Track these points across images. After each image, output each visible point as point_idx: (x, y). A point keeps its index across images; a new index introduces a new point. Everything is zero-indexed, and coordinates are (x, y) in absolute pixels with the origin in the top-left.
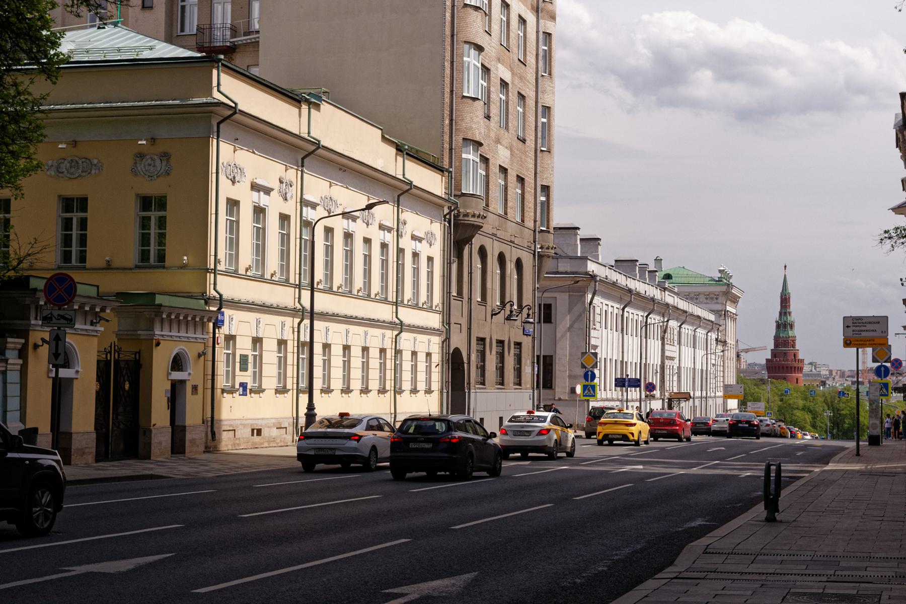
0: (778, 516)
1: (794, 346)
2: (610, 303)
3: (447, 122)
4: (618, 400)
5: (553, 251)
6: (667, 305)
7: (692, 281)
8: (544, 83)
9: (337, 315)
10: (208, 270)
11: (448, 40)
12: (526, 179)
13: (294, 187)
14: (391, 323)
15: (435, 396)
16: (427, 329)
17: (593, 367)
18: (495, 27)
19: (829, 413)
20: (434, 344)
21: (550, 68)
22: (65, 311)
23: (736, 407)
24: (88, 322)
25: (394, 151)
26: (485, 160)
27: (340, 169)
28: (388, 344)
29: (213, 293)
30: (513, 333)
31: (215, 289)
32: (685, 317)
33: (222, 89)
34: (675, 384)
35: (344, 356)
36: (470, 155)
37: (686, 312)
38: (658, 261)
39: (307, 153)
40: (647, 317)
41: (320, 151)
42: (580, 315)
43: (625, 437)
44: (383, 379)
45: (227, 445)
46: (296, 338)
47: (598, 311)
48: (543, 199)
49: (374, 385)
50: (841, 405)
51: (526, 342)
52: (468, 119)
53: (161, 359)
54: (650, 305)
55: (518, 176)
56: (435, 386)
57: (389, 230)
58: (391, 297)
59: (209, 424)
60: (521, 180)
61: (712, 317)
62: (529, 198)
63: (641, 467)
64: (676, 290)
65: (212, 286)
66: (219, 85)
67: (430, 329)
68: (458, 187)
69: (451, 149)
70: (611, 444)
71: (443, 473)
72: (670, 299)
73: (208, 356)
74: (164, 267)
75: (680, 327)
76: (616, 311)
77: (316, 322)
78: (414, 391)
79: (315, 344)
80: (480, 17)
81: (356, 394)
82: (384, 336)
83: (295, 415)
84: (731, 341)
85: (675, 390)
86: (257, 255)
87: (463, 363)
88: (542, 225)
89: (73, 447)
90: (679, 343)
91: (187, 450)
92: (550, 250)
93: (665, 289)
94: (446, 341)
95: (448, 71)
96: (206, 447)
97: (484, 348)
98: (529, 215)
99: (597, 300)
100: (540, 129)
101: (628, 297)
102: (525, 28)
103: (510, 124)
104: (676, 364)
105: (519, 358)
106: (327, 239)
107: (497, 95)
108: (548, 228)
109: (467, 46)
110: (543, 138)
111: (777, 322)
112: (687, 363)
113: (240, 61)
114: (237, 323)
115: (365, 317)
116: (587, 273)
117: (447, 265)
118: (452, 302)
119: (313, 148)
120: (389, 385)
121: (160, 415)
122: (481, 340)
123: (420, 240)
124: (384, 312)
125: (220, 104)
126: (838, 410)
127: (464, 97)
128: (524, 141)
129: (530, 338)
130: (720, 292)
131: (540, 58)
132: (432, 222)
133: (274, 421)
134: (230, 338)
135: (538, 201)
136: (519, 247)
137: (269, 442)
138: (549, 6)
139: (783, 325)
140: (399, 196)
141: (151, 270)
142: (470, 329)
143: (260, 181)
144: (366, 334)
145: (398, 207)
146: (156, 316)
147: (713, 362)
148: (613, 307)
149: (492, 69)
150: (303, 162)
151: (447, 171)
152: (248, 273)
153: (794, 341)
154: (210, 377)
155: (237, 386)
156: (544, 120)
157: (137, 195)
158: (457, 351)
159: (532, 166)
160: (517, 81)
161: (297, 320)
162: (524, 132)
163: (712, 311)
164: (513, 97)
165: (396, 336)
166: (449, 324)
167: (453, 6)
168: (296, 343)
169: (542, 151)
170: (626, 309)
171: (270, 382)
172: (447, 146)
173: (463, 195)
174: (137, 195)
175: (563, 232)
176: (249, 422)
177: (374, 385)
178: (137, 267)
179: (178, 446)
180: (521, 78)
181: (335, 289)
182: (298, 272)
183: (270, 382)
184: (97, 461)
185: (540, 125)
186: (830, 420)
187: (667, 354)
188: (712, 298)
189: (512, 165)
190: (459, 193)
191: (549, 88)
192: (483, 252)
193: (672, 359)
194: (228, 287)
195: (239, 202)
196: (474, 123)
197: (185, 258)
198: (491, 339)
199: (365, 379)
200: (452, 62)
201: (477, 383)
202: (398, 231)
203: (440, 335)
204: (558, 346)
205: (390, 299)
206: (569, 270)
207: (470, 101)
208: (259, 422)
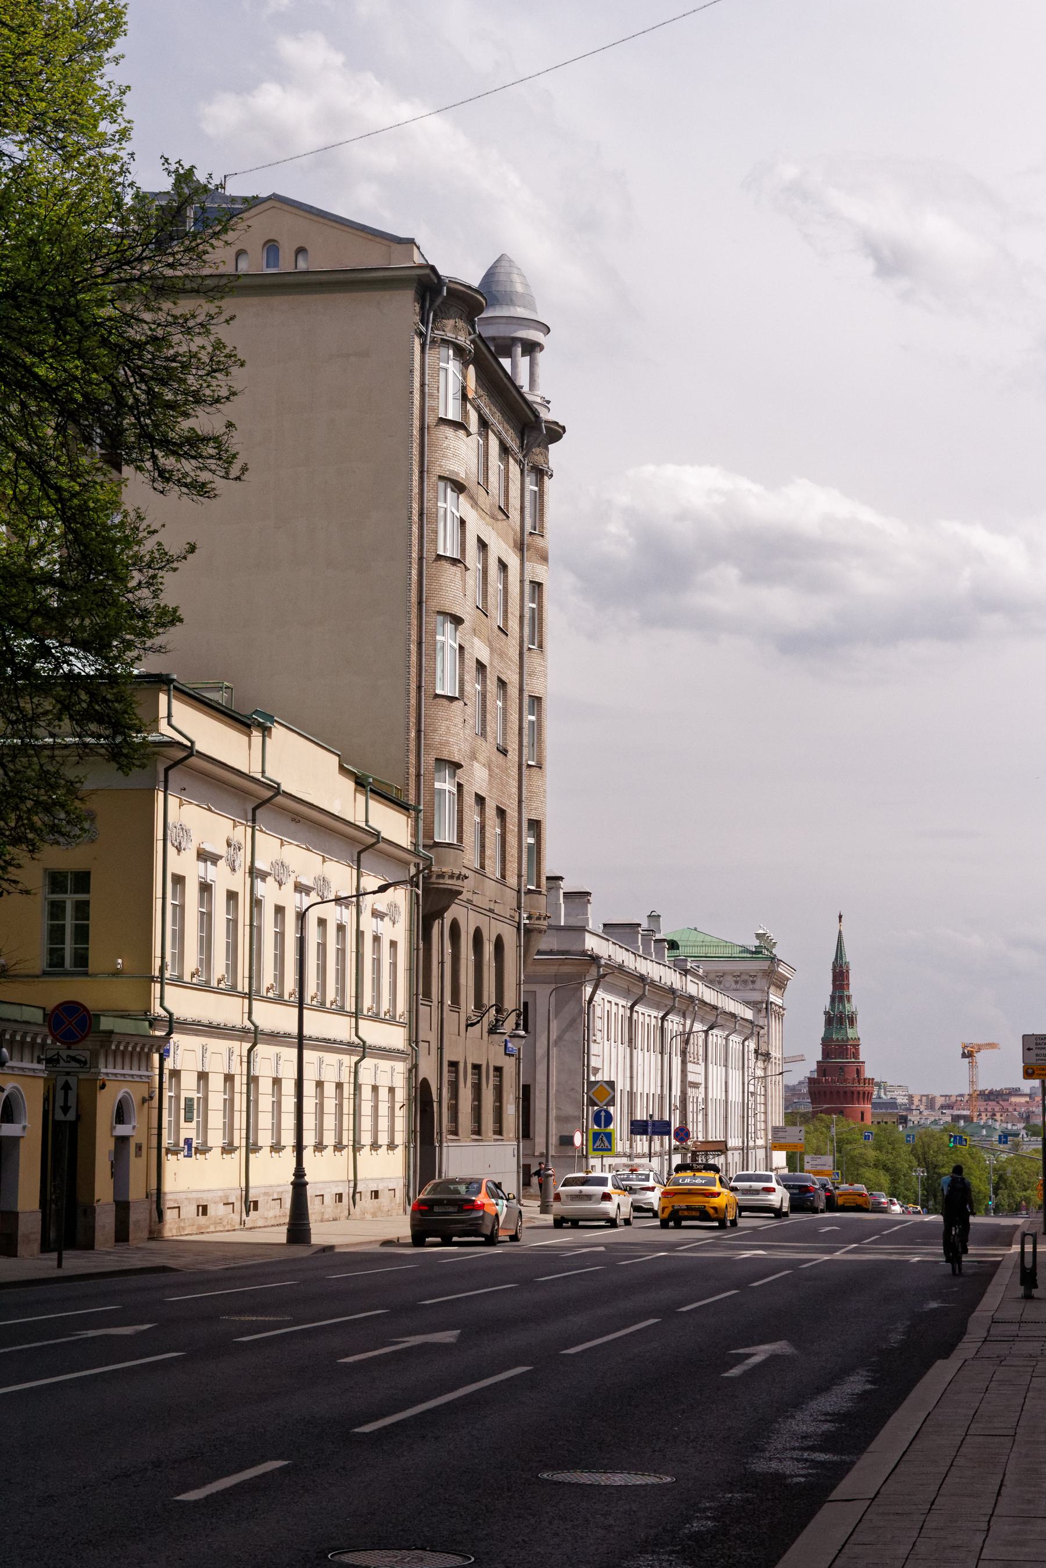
0: (1035, 1292)
1: (856, 1055)
2: (614, 999)
3: (413, 734)
4: (625, 1155)
5: (545, 923)
6: (691, 998)
7: (711, 952)
8: (532, 660)
10: (152, 979)
11: (414, 610)
12: (508, 811)
14: (349, 1044)
15: (400, 1152)
17: (608, 1105)
19: (921, 1173)
22: (81, 1051)
23: (784, 1164)
24: (35, 1061)
25: (351, 785)
27: (293, 820)
31: (162, 1005)
32: (716, 1018)
33: (174, 722)
36: (445, 785)
37: (715, 1008)
38: (654, 918)
39: (259, 801)
40: (663, 1019)
41: (193, 760)
42: (573, 1021)
43: (703, 1215)
44: (229, 1128)
45: (171, 1230)
46: (245, 1072)
47: (598, 1012)
48: (531, 840)
50: (940, 1157)
53: (105, 1105)
54: (672, 1001)
56: (400, 1138)
59: (154, 1198)
61: (749, 1014)
62: (512, 840)
65: (158, 1001)
66: (169, 716)
68: (429, 833)
69: (418, 775)
70: (678, 1226)
73: (153, 1099)
74: (86, 974)
77: (306, 1052)
78: (375, 1146)
79: (305, 1082)
80: (459, 574)
83: (243, 1185)
84: (775, 1053)
87: (432, 1101)
88: (529, 882)
89: (20, 1233)
91: (131, 1238)
92: (542, 922)
94: (414, 1069)
95: (414, 658)
96: (151, 1232)
98: (512, 866)
100: (526, 731)
101: (639, 989)
103: (488, 729)
108: (538, 886)
109: (440, 618)
111: (826, 1013)
112: (716, 1092)
114: (186, 1053)
116: (584, 953)
117: (413, 950)
119: (270, 794)
120: (239, 1139)
121: (103, 1190)
122: (454, 1065)
125: (173, 744)
126: (936, 1166)
127: (437, 696)
128: (504, 752)
129: (513, 1059)
130: (759, 970)
131: (526, 621)
132: (324, 861)
133: (220, 1193)
134: (175, 1074)
135: (524, 845)
136: (499, 918)
137: (215, 1224)
139: (838, 1018)
140: (359, 853)
141: (68, 979)
142: (441, 1048)
145: (358, 869)
146: (101, 1046)
147: (751, 1089)
152: (221, 986)
153: (856, 1047)
154: (155, 1131)
155: (182, 1144)
157: (45, 870)
159: (515, 790)
161: (247, 1046)
163: (747, 1003)
164: (492, 686)
165: (356, 1064)
167: (421, 559)
169: (529, 766)
171: (216, 1139)
172: (412, 771)
173: (437, 845)
174: (45, 870)
176: (194, 1195)
178: (45, 973)
179: (122, 1234)
180: (502, 655)
181: (214, 983)
183: (216, 1139)
184: (42, 1252)
185: (525, 725)
186: (923, 1185)
187: (691, 1078)
188: (745, 982)
189: (490, 791)
190: (431, 842)
191: (539, 668)
193: (696, 1085)
194: (181, 1002)
197: (120, 961)
198: (465, 1063)
200: (420, 644)
203: (404, 1060)
206: (555, 947)
207: (445, 702)
208: (205, 1195)
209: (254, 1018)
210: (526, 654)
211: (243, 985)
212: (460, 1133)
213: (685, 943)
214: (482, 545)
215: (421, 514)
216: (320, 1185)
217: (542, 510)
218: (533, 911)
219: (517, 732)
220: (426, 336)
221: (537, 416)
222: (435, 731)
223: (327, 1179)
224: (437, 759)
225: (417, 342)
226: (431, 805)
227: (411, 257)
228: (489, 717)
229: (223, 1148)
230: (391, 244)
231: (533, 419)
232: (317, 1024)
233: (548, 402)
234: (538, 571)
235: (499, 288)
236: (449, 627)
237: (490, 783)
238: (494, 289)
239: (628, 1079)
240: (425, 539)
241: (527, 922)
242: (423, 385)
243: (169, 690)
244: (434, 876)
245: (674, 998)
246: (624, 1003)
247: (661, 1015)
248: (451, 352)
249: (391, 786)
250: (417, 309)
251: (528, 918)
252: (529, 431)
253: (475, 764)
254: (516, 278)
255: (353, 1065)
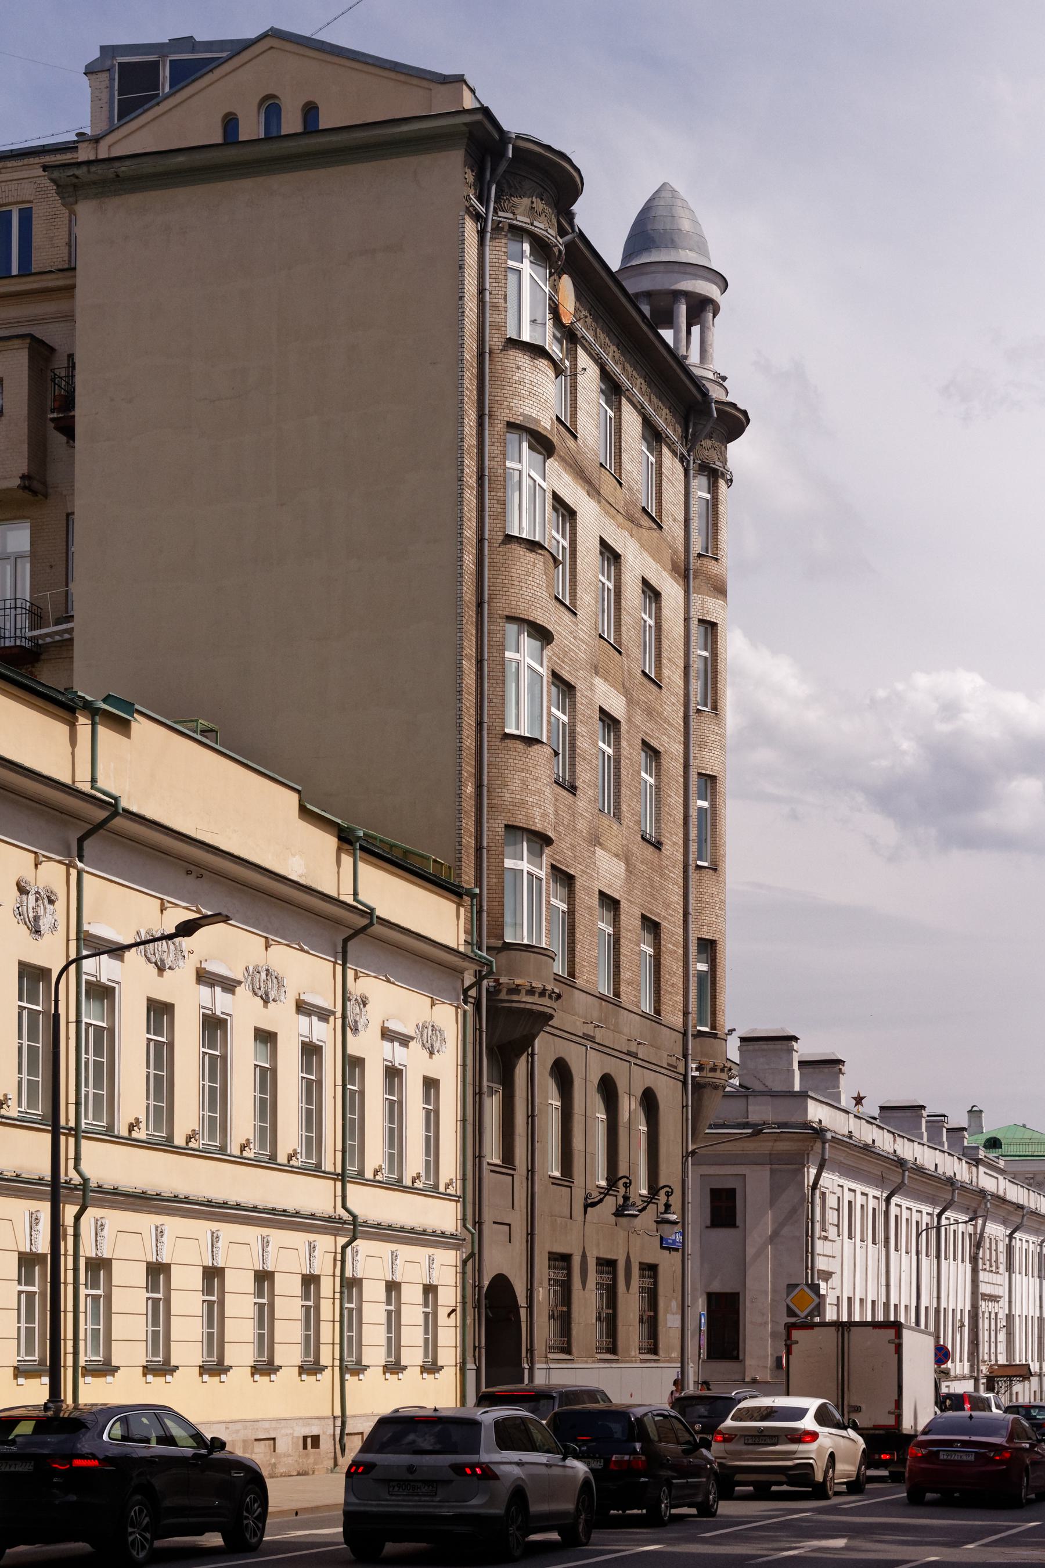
2: (859, 1188)
3: (469, 789)
6: (982, 1193)
8: (703, 727)
9: (187, 1200)
11: (470, 614)
12: (664, 924)
13: (60, 904)
14: (330, 1219)
15: (449, 1377)
16: (424, 1232)
18: (587, 599)
20: (445, 1267)
21: (715, 693)
26: (564, 878)
27: (189, 872)
28: (324, 1266)
29: (73, 1174)
30: (639, 1242)
31: (76, 1167)
34: (1002, 1347)
35: (389, 1302)
36: (521, 862)
37: (1021, 1207)
38: (975, 1113)
41: (119, 822)
46: (338, 1272)
47: (832, 1201)
48: (703, 967)
49: (289, 1353)
51: (668, 1263)
52: (516, 784)
54: (943, 1192)
55: (644, 917)
56: (448, 1356)
57: (324, 1015)
58: (330, 1162)
60: (652, 926)
62: (672, 965)
63: (841, 1543)
64: (1002, 1164)
65: (71, 1163)
67: (434, 1233)
69: (479, 849)
71: (635, 1511)
72: (987, 1182)
75: (1011, 1236)
76: (872, 1203)
80: (540, 565)
81: (239, 1376)
82: (312, 1248)
85: (1002, 1360)
86: (263, 1119)
87: (517, 1307)
90: (1010, 1268)
92: (718, 1074)
93: (978, 1162)
94: (473, 1261)
95: (469, 680)
97: (569, 1275)
98: (672, 1001)
99: (830, 1180)
100: (693, 821)
101: (897, 1177)
102: (659, 609)
103: (624, 807)
104: (1001, 1309)
105: (652, 1298)
106: (427, 1100)
107: (593, 744)
109: (512, 628)
110: (701, 841)
113: (48, 676)
115: (261, 1204)
116: (807, 1125)
118: (488, 1178)
119: (103, 814)
123: (404, 1040)
124: (315, 1196)
127: (507, 736)
128: (658, 845)
129: (678, 1255)
132: (433, 1004)
136: (647, 1065)
138: (712, 567)
140: (345, 941)
142: (531, 1235)
143: (212, 967)
144: (394, 1256)
145: (344, 965)
148: (867, 1196)
149: (580, 685)
150: (80, 849)
151: (473, 896)
156: (704, 804)
158: (501, 1282)
159: (677, 899)
160: (639, 718)
162: (658, 828)
165: (344, 1248)
166: (479, 1223)
167: (480, 540)
168: (338, 1280)
170: (895, 1200)
172: (469, 841)
175: (764, 1045)
177: (289, 1353)
180: (650, 712)
182: (339, 1147)
185: (693, 813)
189: (629, 892)
190: (499, 943)
191: (712, 737)
192: (562, 1072)
193: (994, 1298)
195: (438, 1080)
196: (532, 791)
198: (584, 1256)
199: (394, 1345)
200: (480, 662)
201: (552, 1349)
202: (344, 1017)
203: (456, 1247)
204: (750, 1273)
205: (328, 1166)
207: (520, 746)
209: (84, 1166)
210: (693, 717)
211: (330, 1162)
212: (574, 1350)
213: (1009, 1141)
214: (610, 555)
215: (481, 478)
216: (267, 1425)
217: (715, 524)
218: (704, 1060)
219: (681, 822)
220: (486, 220)
221: (705, 394)
222: (504, 785)
223: (287, 1415)
224: (507, 826)
225: (470, 228)
226: (499, 891)
227: (460, 98)
228: (624, 790)
229: (16, 1368)
230: (432, 86)
231: (699, 397)
232: (369, 1203)
233: (724, 379)
234: (710, 607)
235: (657, 227)
236: (527, 642)
237: (628, 880)
238: (649, 227)
239: (884, 1288)
240: (487, 514)
241: (697, 1074)
242: (481, 291)
243: (354, 850)
244: (504, 991)
245: (954, 1190)
246: (878, 1194)
247: (937, 1211)
248: (526, 247)
249: (428, 858)
250: (470, 177)
251: (697, 1069)
252: (699, 421)
253: (599, 851)
254: (679, 212)
255: (339, 1250)
